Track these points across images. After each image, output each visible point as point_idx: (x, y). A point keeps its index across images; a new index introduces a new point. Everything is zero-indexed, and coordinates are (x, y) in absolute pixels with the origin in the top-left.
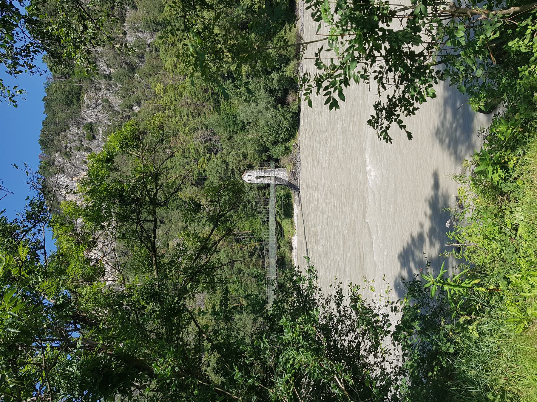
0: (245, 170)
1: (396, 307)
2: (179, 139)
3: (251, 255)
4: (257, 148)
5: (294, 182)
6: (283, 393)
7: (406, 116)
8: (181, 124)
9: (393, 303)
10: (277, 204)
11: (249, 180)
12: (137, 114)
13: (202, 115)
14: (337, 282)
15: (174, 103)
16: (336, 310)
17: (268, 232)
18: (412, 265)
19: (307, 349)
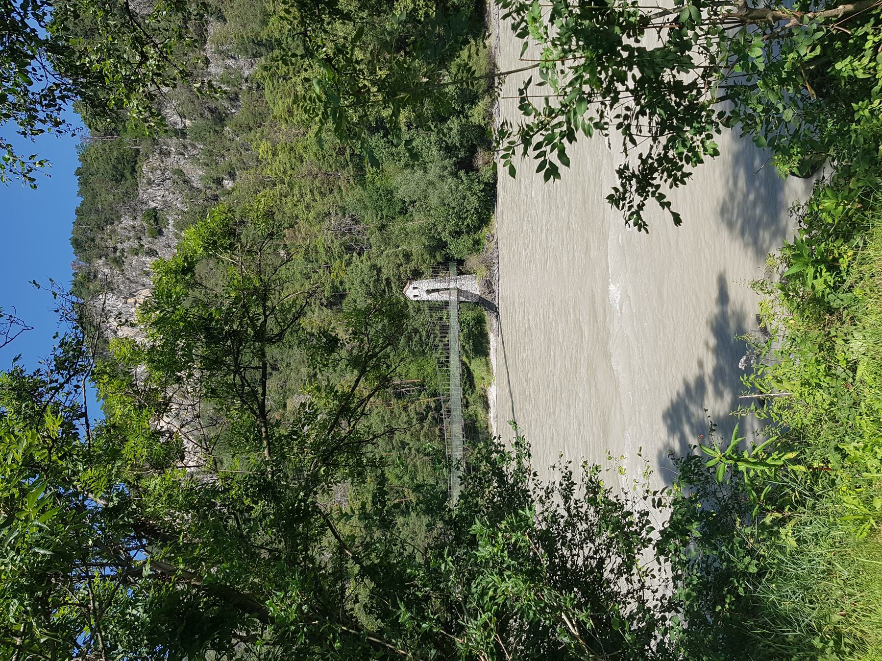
0: (408, 279)
1: (660, 500)
2: (300, 232)
3: (422, 419)
5: (489, 298)
6: (478, 643)
7: (671, 187)
8: (301, 206)
9: (655, 493)
11: (415, 296)
12: (229, 193)
13: (336, 191)
15: (289, 173)
17: (448, 380)
18: (687, 429)
19: (517, 572)
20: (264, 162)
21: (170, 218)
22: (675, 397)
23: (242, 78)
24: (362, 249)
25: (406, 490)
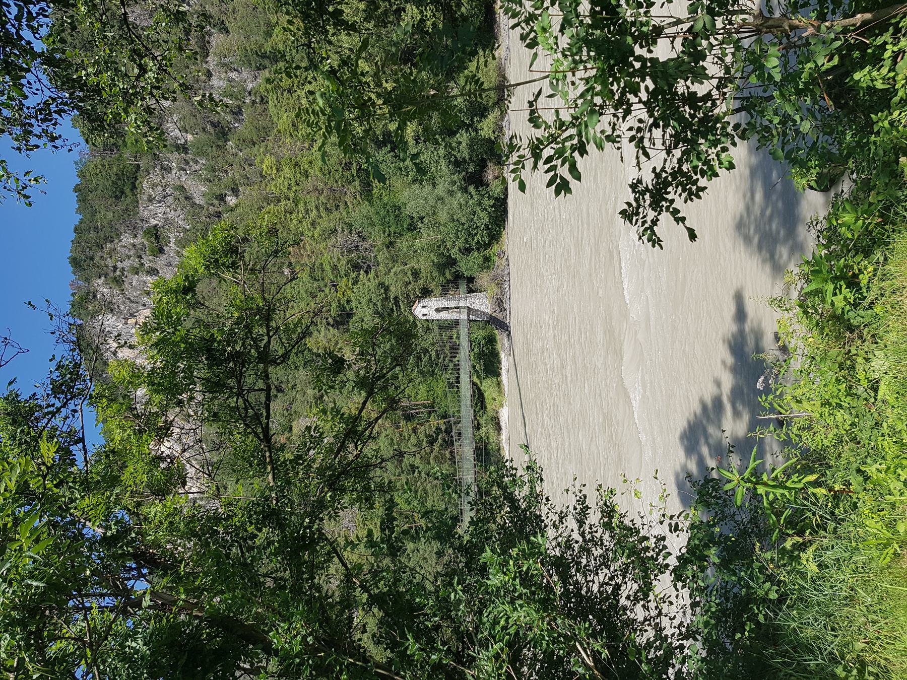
0: (417, 297)
1: (677, 524)
3: (431, 442)
4: (436, 261)
5: (500, 316)
6: (490, 675)
7: (686, 202)
8: (306, 223)
9: (672, 517)
11: (424, 315)
12: (232, 210)
13: (342, 207)
14: (578, 484)
15: (294, 189)
17: (459, 401)
18: (705, 451)
20: (269, 178)
22: (692, 418)
23: (245, 91)
24: (369, 267)
25: (415, 514)
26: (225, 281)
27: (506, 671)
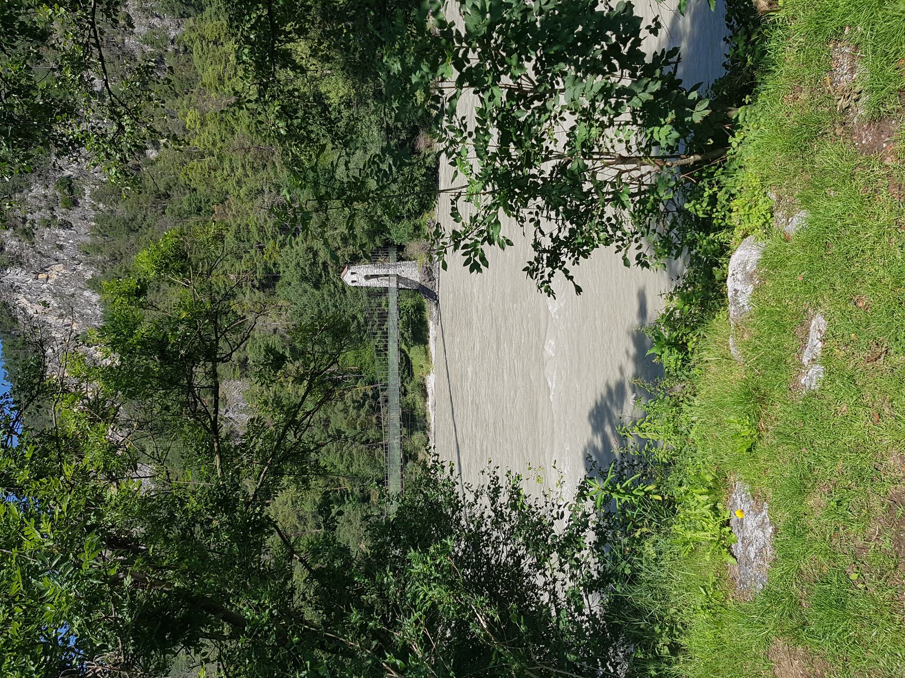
1: (563, 513)
5: (429, 285)
6: (411, 636)
7: (574, 264)
8: (232, 182)
9: (559, 507)
10: (400, 321)
11: (353, 282)
12: (152, 163)
13: (269, 167)
14: (492, 466)
15: (219, 145)
16: (489, 506)
18: (608, 429)
20: (192, 132)
21: (86, 188)
23: (167, 38)
25: (341, 478)
26: (175, 284)
27: (423, 633)
